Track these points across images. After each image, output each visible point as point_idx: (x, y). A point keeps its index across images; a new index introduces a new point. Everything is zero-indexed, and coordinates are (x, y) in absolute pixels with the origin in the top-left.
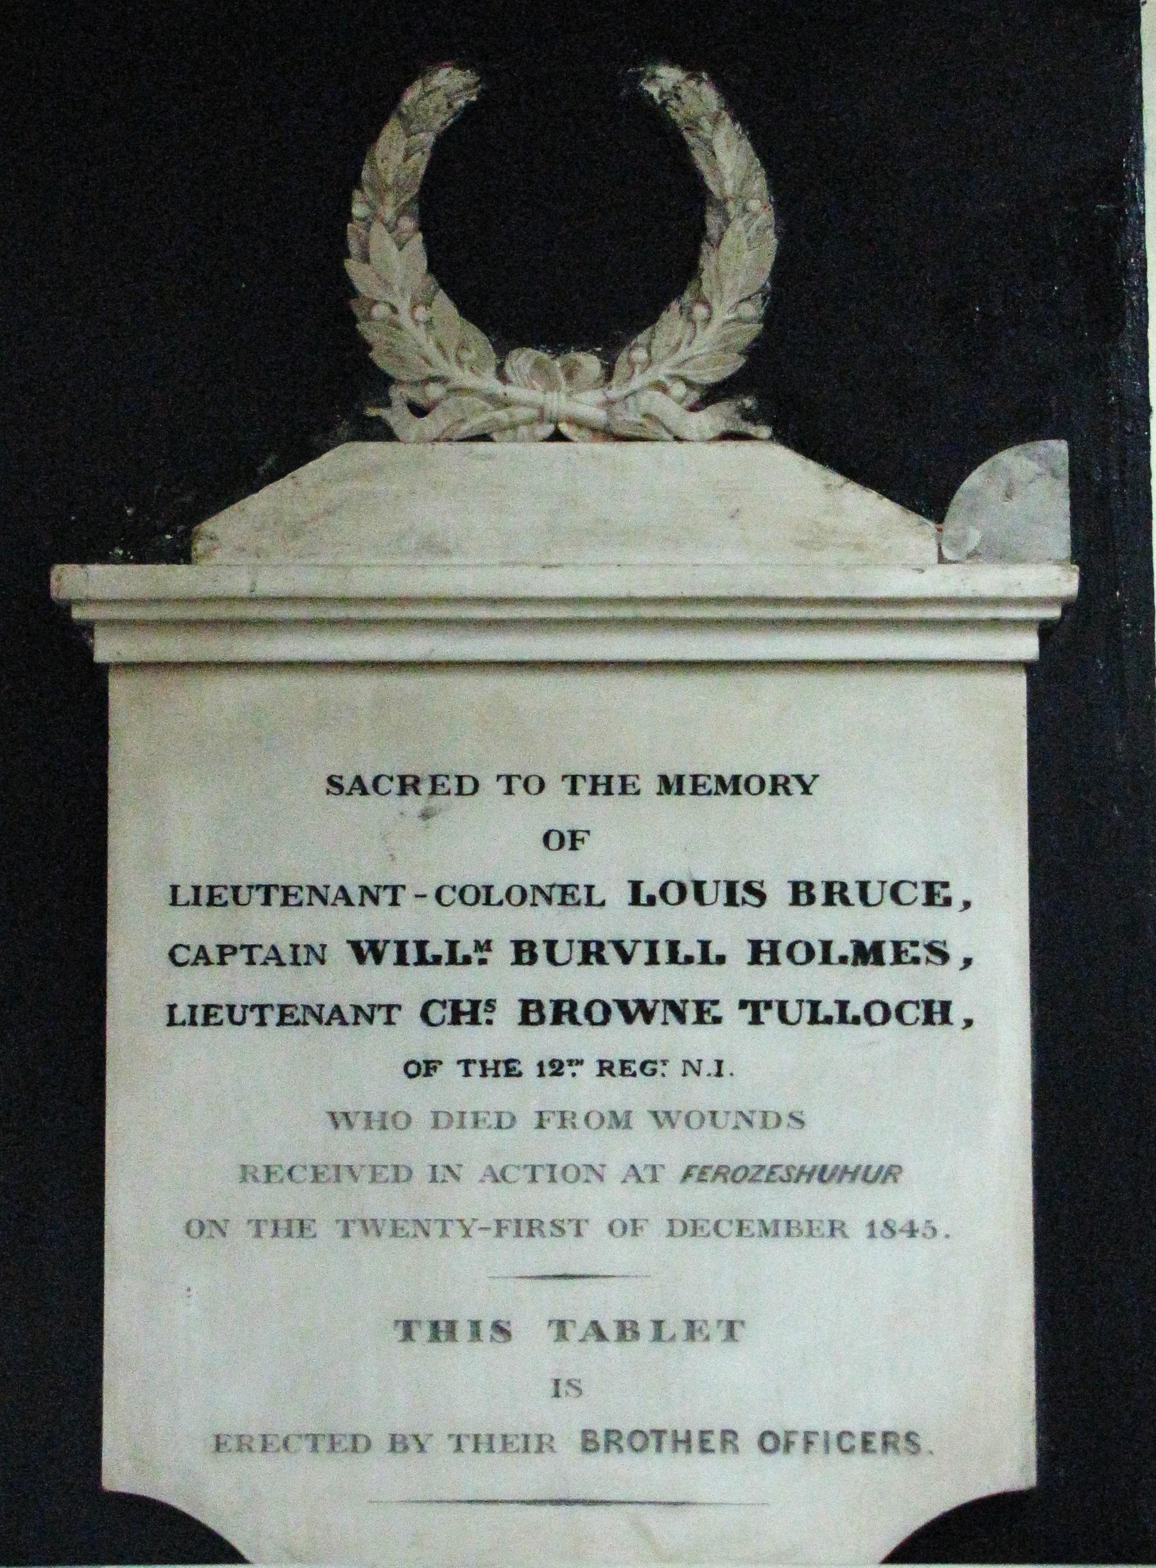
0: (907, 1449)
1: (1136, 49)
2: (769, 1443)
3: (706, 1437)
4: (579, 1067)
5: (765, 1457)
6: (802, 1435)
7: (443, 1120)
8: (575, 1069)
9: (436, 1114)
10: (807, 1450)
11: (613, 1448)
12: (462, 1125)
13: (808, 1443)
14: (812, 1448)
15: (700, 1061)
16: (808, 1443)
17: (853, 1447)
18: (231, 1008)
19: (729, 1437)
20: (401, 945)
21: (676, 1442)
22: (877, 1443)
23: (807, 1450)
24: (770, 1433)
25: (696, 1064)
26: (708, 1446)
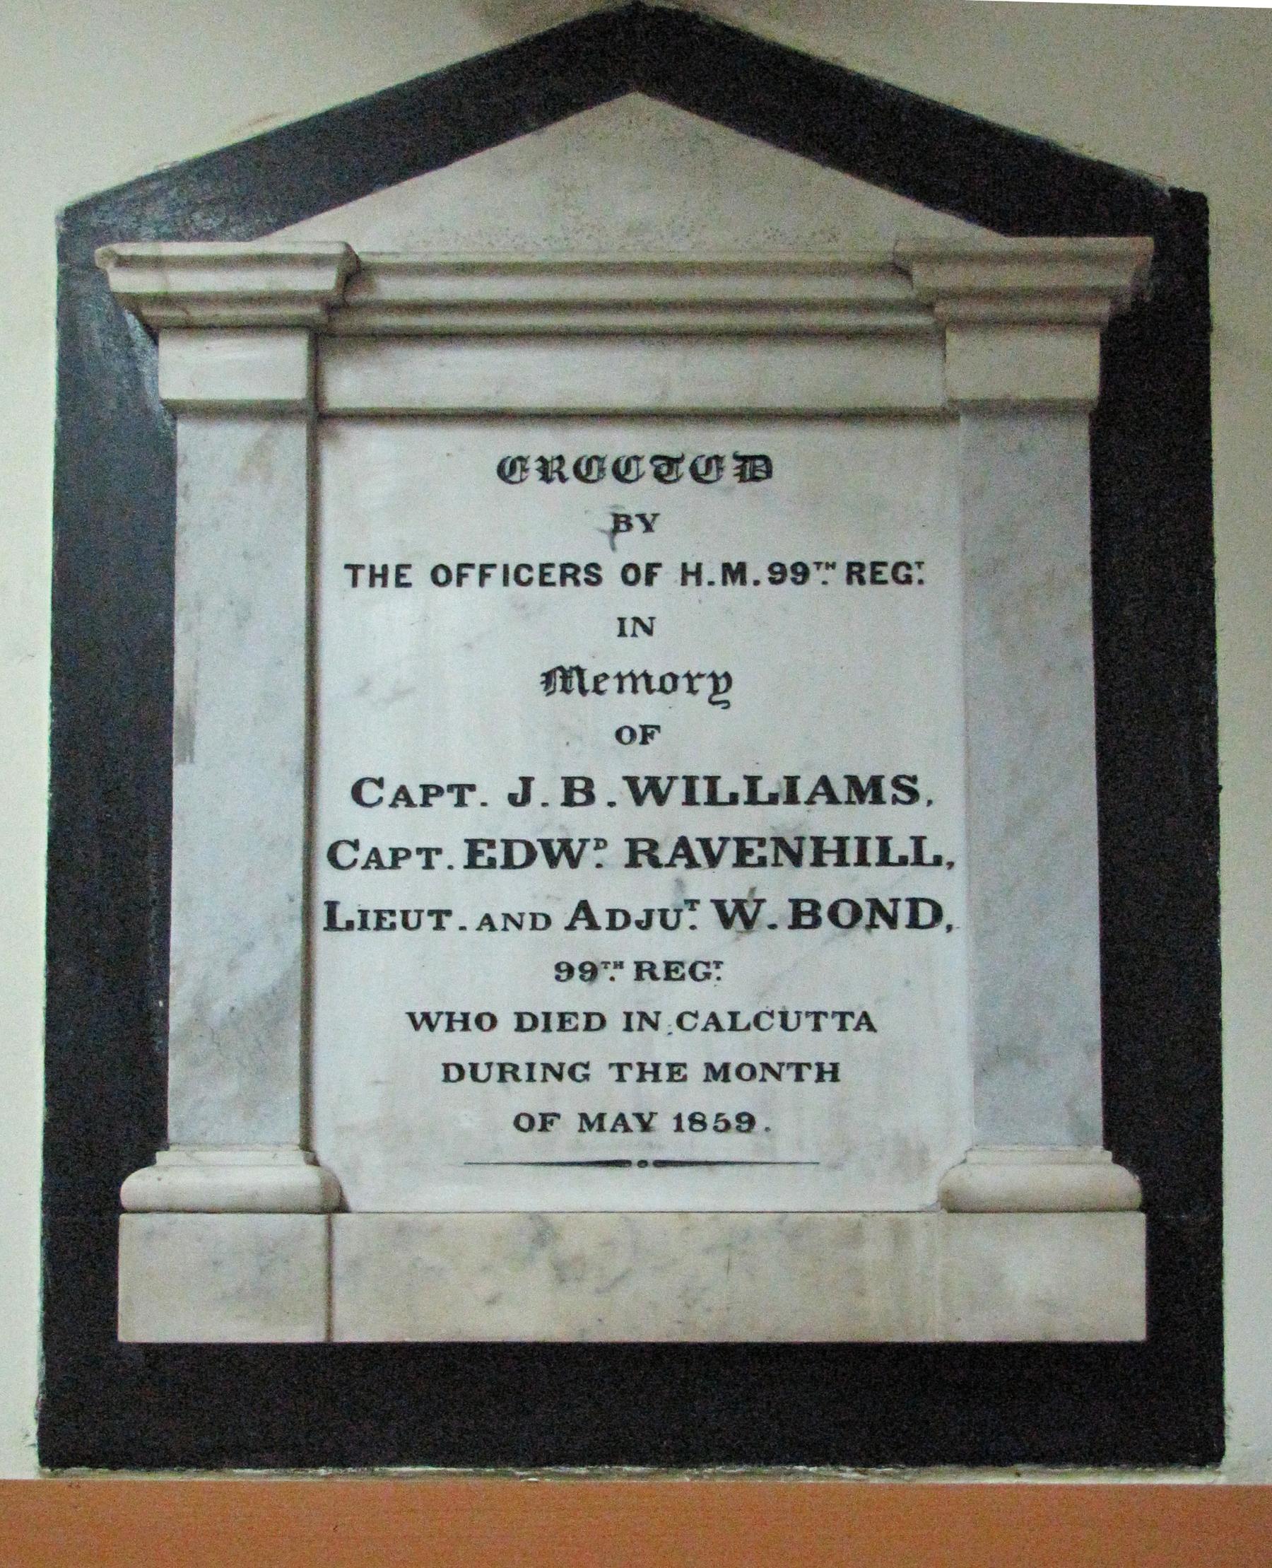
0: (587, 581)
1: (1204, 483)
2: (442, 576)
3: (547, 570)
4: (618, 970)
5: (437, 588)
6: (477, 568)
7: (528, 1022)
8: (611, 971)
9: (446, 1067)
10: (482, 583)
11: (569, 581)
12: (547, 1028)
13: (483, 576)
14: (487, 580)
15: (658, 1013)
16: (483, 576)
17: (531, 579)
18: (405, 913)
19: (570, 571)
20: (690, 781)
21: (373, 576)
22: (555, 575)
23: (482, 583)
24: (442, 566)
25: (653, 1017)
26: (547, 579)
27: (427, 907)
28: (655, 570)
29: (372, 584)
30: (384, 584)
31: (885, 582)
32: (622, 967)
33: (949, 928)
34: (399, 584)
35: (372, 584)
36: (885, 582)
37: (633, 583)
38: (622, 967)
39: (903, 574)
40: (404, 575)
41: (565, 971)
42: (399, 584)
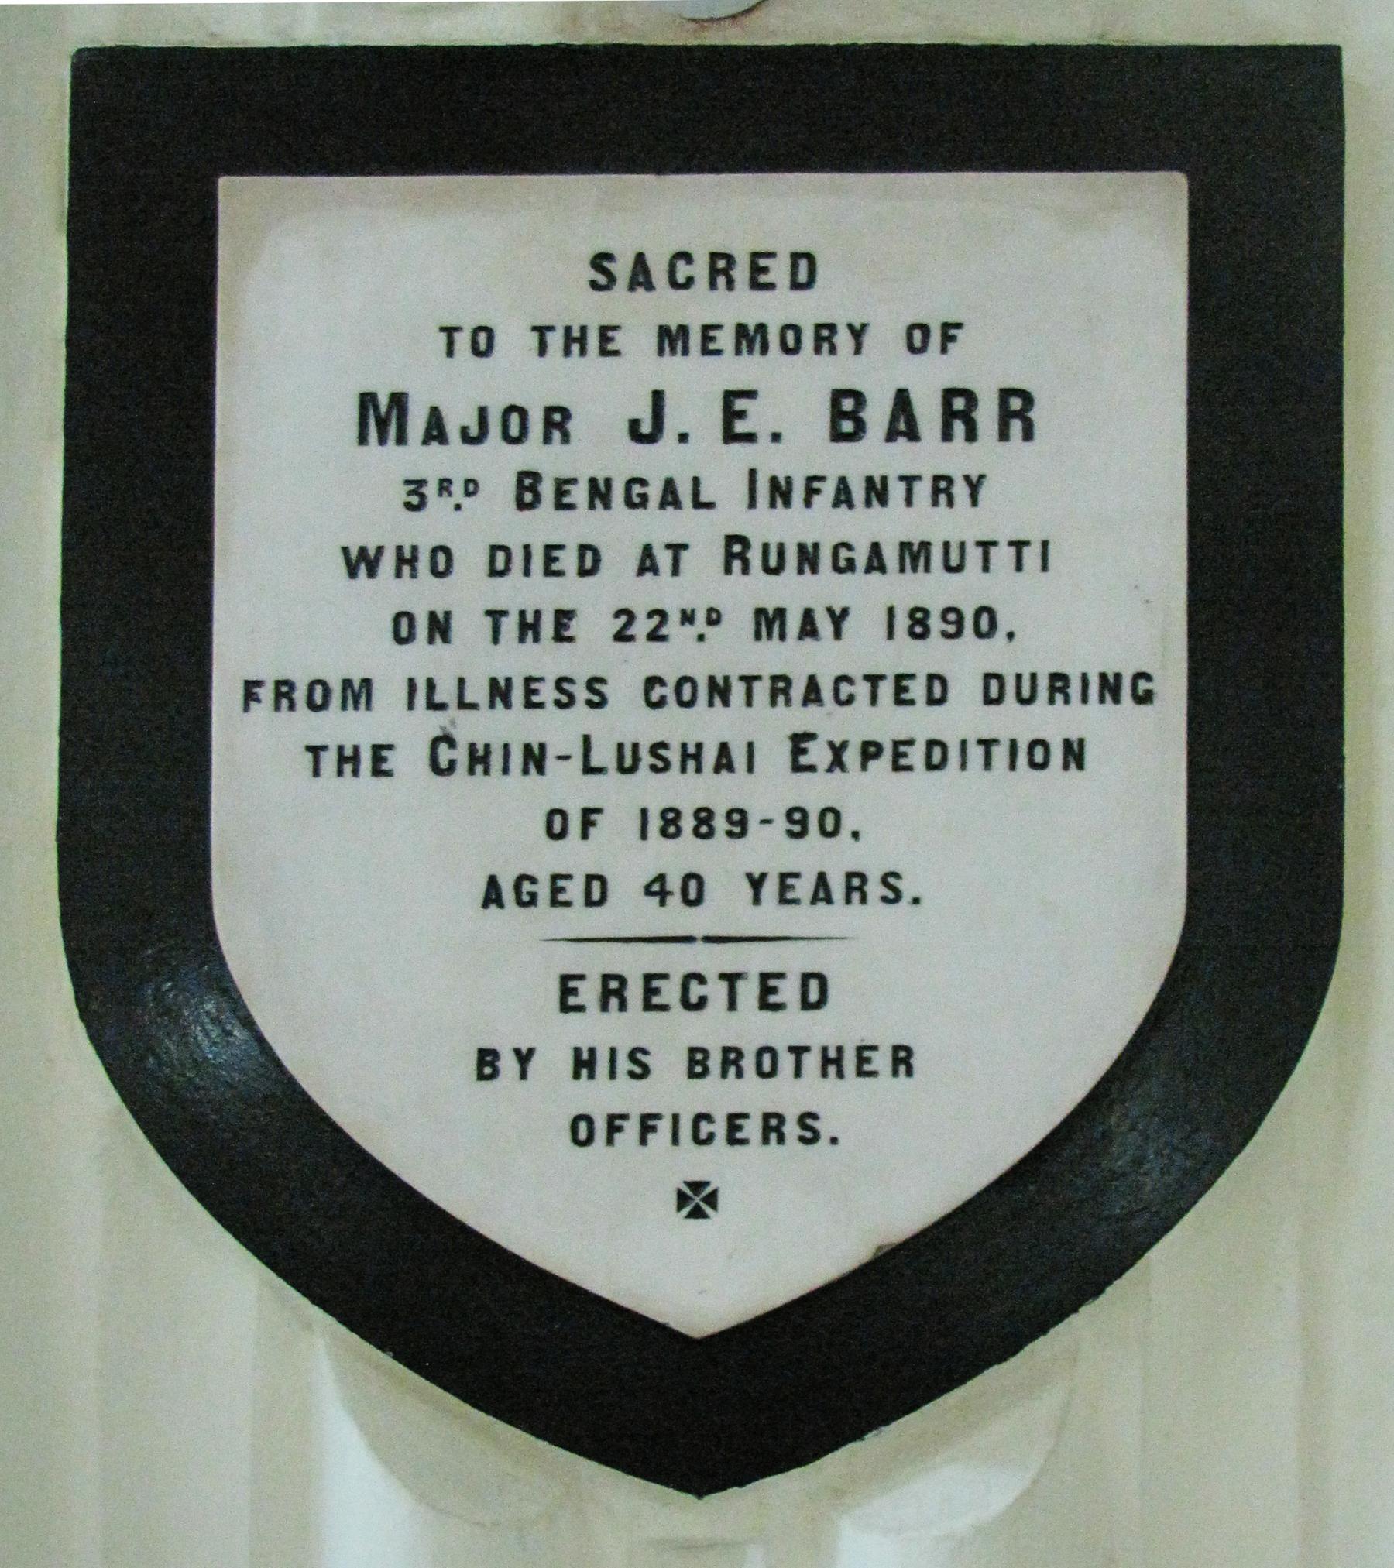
10: (643, 1141)
14: (592, 831)
17: (452, 764)
23: (643, 1141)
27: (820, 776)
28: (385, 753)
29: (567, 352)
30: (583, 352)
31: (664, 1008)
32: (664, 332)
33: (683, 438)
34: (604, 352)
35: (567, 352)
36: (664, 1008)
37: (511, 409)
38: (664, 332)
39: (560, 758)
40: (741, 415)
41: (831, 823)
42: (604, 352)
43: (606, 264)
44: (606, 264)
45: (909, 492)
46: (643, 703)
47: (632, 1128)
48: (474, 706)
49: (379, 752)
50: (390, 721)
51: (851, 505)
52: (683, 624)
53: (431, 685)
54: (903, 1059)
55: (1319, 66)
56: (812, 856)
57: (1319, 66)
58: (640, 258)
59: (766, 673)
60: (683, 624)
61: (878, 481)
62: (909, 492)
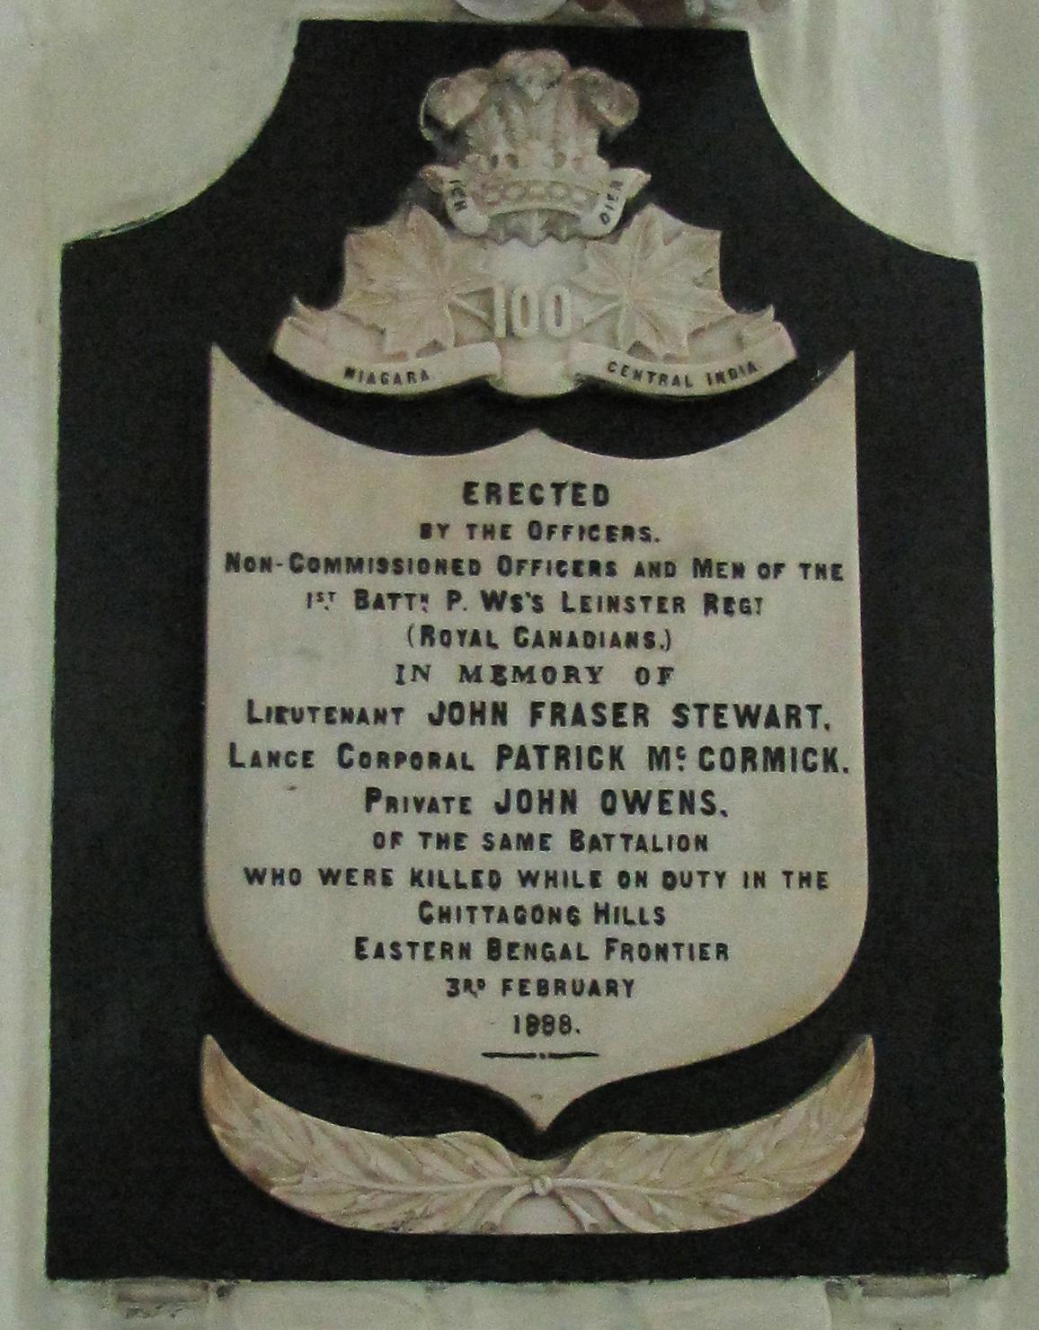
23: (534, 574)
43: (600, 710)
44: (600, 710)
45: (701, 717)
46: (697, 764)
47: (528, 567)
48: (241, 765)
49: (307, 755)
50: (689, 586)
51: (415, 799)
52: (228, 569)
53: (441, 874)
54: (722, 950)
55: (984, 1253)
56: (691, 861)
57: (984, 1253)
58: (572, 634)
59: (677, 789)
60: (228, 569)
61: (530, 957)
62: (701, 717)
